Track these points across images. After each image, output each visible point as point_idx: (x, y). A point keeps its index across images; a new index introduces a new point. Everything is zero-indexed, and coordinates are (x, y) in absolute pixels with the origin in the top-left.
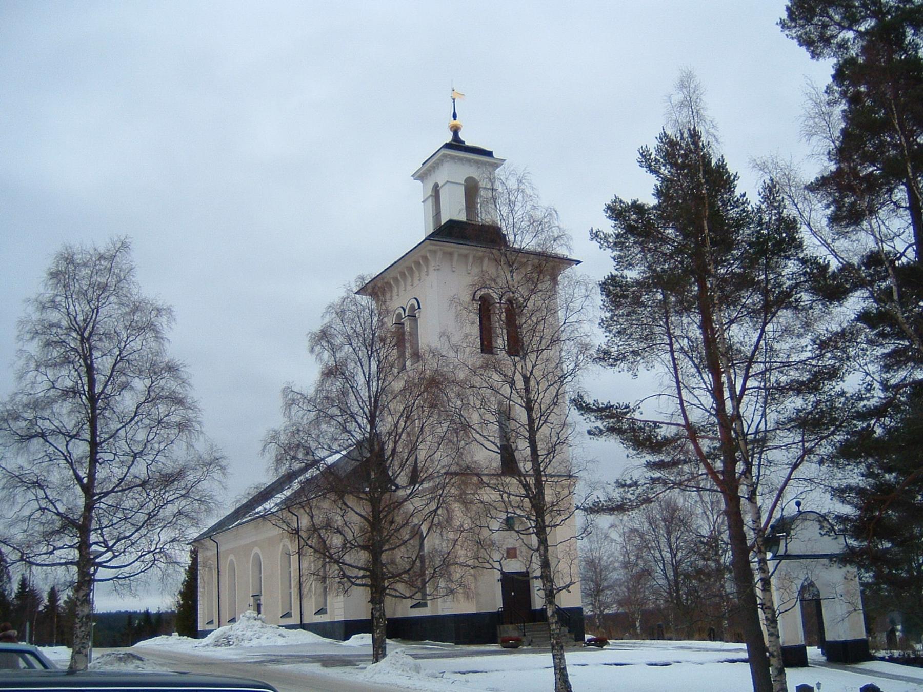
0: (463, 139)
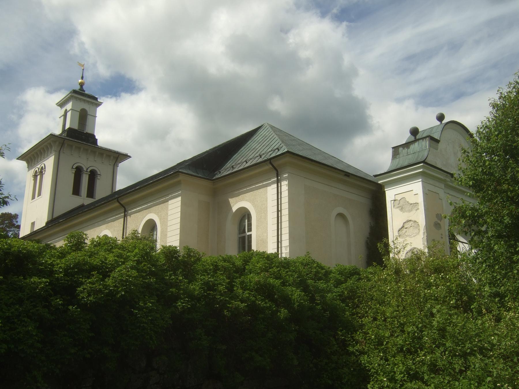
0: (85, 89)
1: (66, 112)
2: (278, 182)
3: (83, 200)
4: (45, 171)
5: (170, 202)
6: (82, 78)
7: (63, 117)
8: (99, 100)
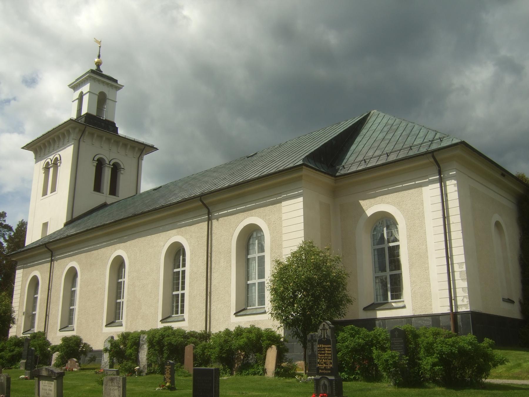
0: (102, 70)
1: (81, 96)
2: (441, 181)
3: (105, 197)
4: (61, 163)
5: (284, 203)
6: (99, 57)
7: (77, 101)
8: (119, 82)
